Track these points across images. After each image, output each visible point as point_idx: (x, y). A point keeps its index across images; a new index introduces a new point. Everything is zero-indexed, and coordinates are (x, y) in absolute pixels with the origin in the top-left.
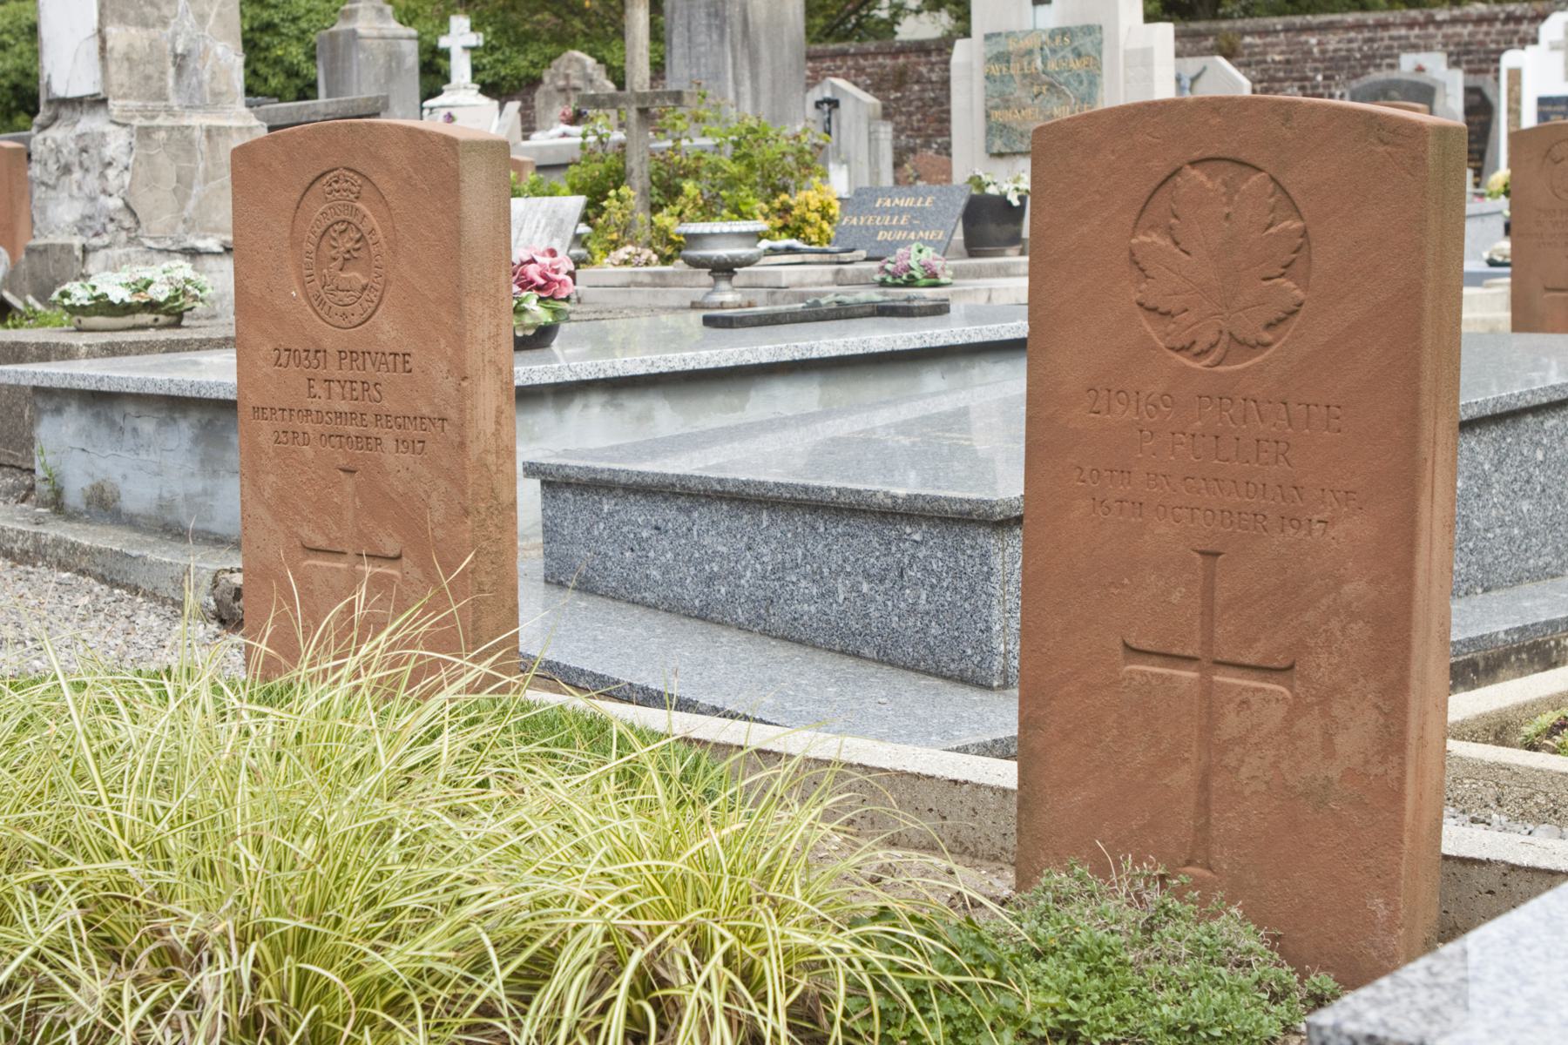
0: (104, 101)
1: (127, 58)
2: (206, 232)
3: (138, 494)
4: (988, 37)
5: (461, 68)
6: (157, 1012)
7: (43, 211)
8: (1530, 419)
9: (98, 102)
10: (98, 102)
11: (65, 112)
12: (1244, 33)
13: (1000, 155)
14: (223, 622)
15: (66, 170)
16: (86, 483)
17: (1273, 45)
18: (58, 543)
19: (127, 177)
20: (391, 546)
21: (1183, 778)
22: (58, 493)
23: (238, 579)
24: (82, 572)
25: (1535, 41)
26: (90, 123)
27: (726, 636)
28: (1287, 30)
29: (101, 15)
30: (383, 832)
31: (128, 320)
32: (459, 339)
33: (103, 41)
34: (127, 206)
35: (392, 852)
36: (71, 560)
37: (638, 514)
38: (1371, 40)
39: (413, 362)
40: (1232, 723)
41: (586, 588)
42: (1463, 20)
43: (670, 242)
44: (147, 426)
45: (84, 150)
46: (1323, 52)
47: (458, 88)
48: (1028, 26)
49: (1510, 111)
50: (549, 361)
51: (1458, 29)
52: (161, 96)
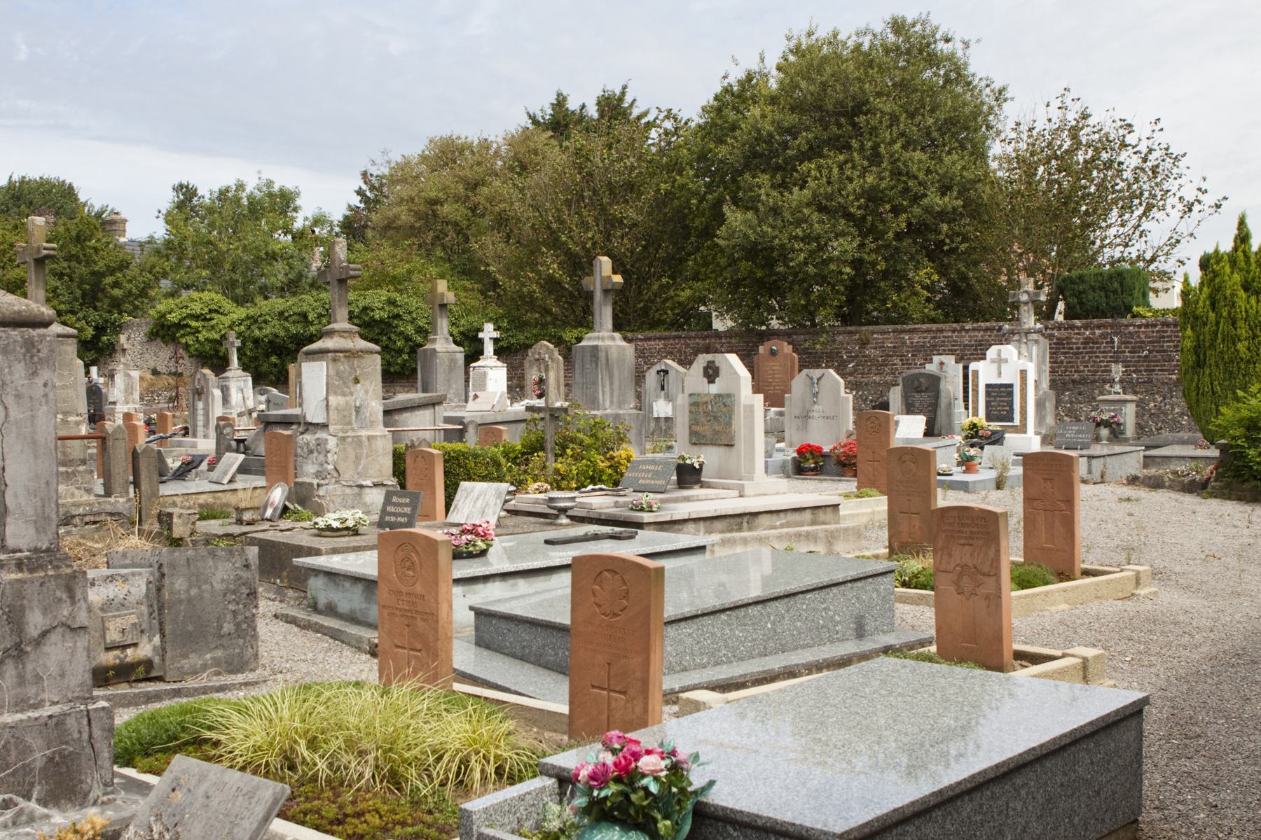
0: (327, 426)
1: (337, 409)
2: (366, 478)
3: (344, 606)
4: (690, 395)
5: (489, 348)
6: (359, 764)
7: (301, 467)
8: (800, 596)
9: (324, 426)
10: (324, 426)
11: (311, 428)
12: (874, 332)
13: (695, 444)
14: (372, 655)
15: (311, 452)
16: (326, 601)
17: (888, 339)
18: (316, 623)
19: (336, 457)
20: (419, 647)
21: (604, 717)
22: (316, 604)
23: (376, 641)
24: (325, 634)
25: (985, 359)
26: (321, 435)
27: (527, 666)
28: (894, 332)
29: (327, 392)
30: (408, 726)
31: (338, 534)
32: (437, 593)
33: (328, 402)
34: (336, 469)
35: (410, 731)
36: (319, 629)
37: (503, 625)
38: (935, 338)
39: (426, 598)
40: (614, 704)
41: (488, 647)
42: (979, 330)
43: (560, 474)
44: (347, 584)
45: (319, 445)
46: (912, 343)
47: (487, 358)
48: (706, 392)
49: (973, 390)
50: (484, 565)
51: (976, 333)
52: (350, 423)
